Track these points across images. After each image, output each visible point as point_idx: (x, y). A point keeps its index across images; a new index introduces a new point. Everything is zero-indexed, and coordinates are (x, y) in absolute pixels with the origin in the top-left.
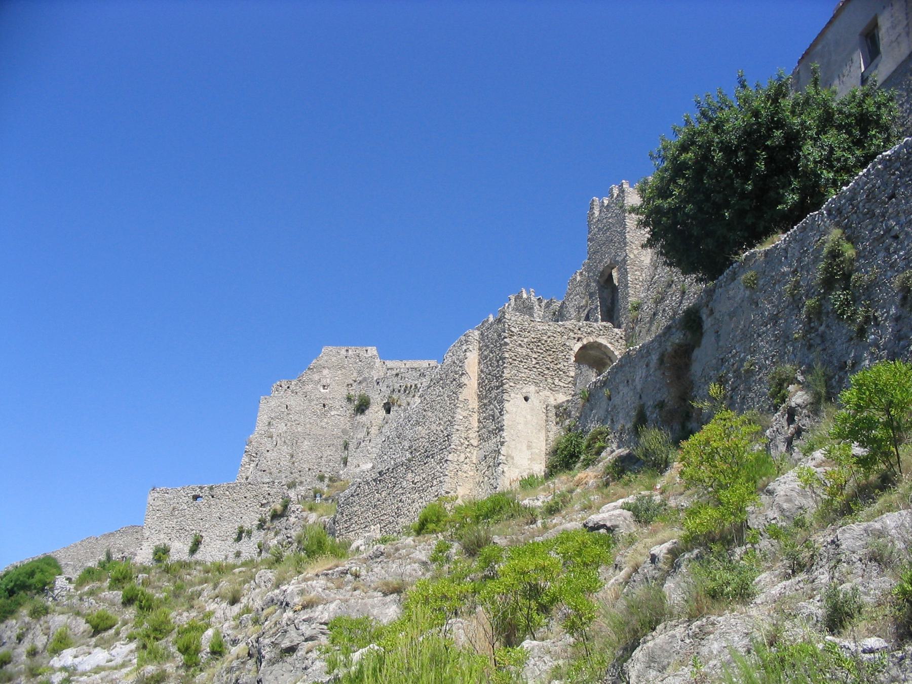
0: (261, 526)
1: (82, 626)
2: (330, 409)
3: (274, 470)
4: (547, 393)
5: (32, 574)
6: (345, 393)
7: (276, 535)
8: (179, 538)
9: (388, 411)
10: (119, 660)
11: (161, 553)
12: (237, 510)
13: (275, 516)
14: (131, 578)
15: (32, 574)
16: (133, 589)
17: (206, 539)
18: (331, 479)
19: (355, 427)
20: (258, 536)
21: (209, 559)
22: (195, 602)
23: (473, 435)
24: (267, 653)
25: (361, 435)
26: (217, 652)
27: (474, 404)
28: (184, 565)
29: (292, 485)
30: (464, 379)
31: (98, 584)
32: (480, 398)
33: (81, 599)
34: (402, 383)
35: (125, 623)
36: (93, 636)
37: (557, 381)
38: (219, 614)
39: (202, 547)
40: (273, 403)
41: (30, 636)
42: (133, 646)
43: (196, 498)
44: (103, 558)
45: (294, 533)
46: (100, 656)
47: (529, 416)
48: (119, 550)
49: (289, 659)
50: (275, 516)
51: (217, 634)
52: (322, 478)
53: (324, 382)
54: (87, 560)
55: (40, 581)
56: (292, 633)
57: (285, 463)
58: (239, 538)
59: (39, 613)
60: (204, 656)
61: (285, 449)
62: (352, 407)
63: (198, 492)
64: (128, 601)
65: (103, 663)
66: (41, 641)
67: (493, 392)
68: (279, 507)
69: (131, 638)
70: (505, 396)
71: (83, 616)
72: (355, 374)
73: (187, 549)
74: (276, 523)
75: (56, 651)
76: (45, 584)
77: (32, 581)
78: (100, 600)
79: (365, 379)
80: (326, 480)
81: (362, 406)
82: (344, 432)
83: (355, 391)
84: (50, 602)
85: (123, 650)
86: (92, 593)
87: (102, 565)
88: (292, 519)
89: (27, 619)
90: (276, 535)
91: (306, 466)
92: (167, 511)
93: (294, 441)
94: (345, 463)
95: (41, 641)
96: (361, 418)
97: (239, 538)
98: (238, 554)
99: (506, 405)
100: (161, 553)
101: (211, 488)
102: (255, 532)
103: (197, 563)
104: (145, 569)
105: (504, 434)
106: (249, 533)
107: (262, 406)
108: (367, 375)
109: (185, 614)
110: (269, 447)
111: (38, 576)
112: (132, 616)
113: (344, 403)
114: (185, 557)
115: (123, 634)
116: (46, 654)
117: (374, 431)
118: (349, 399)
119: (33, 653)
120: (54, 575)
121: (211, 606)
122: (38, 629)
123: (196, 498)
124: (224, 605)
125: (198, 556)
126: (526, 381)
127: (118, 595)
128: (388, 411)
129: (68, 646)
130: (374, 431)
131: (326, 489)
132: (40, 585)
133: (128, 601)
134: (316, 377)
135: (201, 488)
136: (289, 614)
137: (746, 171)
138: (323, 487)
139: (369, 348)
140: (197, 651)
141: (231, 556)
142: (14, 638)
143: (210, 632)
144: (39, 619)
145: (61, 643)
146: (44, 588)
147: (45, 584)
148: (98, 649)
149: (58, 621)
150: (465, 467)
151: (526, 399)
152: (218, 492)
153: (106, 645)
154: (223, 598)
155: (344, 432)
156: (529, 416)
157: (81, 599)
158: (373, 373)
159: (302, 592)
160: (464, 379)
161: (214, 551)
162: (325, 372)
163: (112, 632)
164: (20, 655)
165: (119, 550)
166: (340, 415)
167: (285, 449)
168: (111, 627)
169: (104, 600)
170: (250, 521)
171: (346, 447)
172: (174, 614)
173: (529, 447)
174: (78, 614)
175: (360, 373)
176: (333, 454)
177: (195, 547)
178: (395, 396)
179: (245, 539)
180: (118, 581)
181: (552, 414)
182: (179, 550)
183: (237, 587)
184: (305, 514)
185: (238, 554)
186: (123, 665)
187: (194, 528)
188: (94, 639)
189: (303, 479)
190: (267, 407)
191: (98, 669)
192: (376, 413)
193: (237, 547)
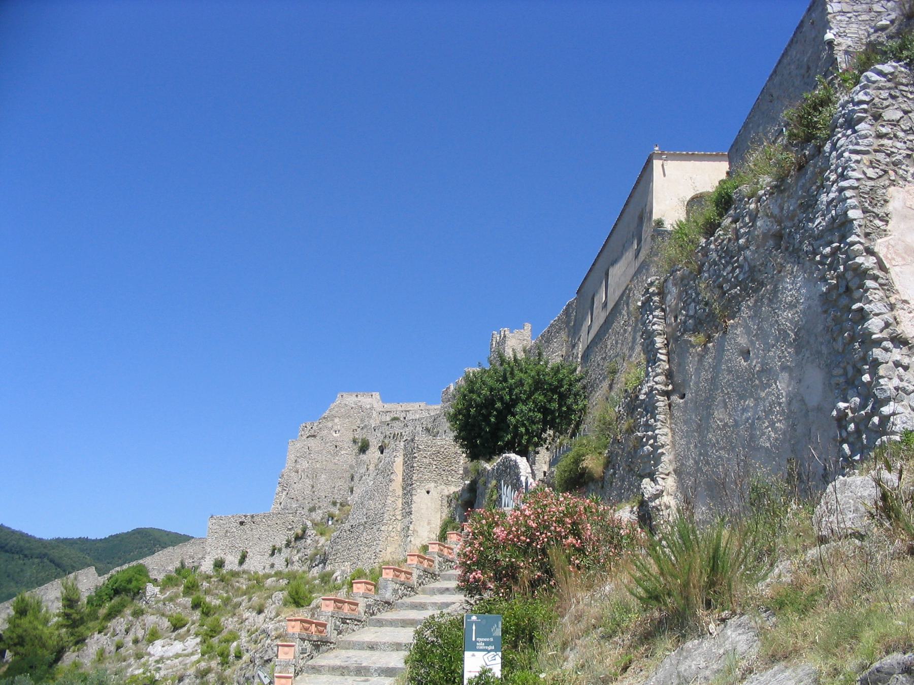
0: (288, 545)
1: (166, 623)
2: (341, 449)
3: (300, 498)
4: (443, 487)
5: (130, 581)
6: (351, 437)
7: (298, 552)
8: (231, 553)
9: (382, 453)
10: (189, 650)
11: (219, 564)
12: (271, 532)
13: (298, 538)
14: (198, 586)
15: (130, 581)
16: (198, 598)
17: (250, 554)
18: (341, 504)
19: (359, 464)
20: (286, 553)
21: (252, 569)
22: (237, 611)
23: (398, 512)
24: (258, 662)
25: (363, 471)
26: (238, 657)
27: (400, 492)
28: (235, 574)
29: (312, 510)
30: (392, 477)
31: (175, 590)
32: (404, 489)
33: (164, 604)
34: (392, 431)
35: (193, 623)
36: (173, 631)
37: (450, 478)
38: (251, 620)
39: (247, 560)
40: (298, 445)
41: (133, 630)
42: (198, 640)
43: (242, 523)
44: (178, 565)
45: (309, 552)
46: (178, 647)
47: (429, 504)
48: (190, 557)
49: (268, 666)
50: (298, 538)
51: (238, 645)
52: (334, 504)
53: (335, 428)
54: (168, 565)
55: (136, 587)
56: (270, 652)
57: (308, 492)
58: (273, 554)
59: (138, 613)
60: (231, 658)
61: (308, 482)
62: (356, 448)
63: (243, 519)
64: (196, 606)
65: (180, 652)
66: (140, 634)
67: (408, 488)
68: (300, 532)
69: (197, 635)
70: (414, 492)
71: (167, 616)
72: (359, 422)
73: (237, 561)
74: (298, 543)
75: (151, 641)
76: (140, 589)
77: (131, 586)
78: (176, 604)
79: (366, 426)
80: (338, 505)
81: (364, 448)
82: (351, 467)
83: (359, 435)
84: (143, 605)
85: (192, 642)
86: (171, 599)
87: (178, 571)
88: (309, 541)
89: (131, 618)
90: (298, 552)
91: (323, 495)
92: (222, 533)
93: (314, 475)
94: (352, 492)
95: (140, 634)
96: (363, 457)
97: (273, 554)
98: (272, 566)
99: (414, 497)
100: (219, 564)
101: (252, 517)
102: (284, 549)
103: (244, 572)
104: (208, 578)
105: (412, 517)
106: (280, 550)
107: (290, 447)
108: (367, 423)
109: (230, 619)
110: (296, 480)
111: (134, 583)
112: (198, 617)
113: (351, 444)
114: (236, 568)
115: (192, 632)
116: (145, 642)
117: (371, 467)
118: (355, 441)
119: (136, 641)
120: (145, 583)
121: (246, 615)
122: (138, 625)
123: (242, 523)
124: (254, 614)
125: (245, 566)
126: (428, 481)
127: (188, 601)
128: (382, 453)
129: (157, 638)
130: (371, 467)
131: (337, 512)
132: (136, 590)
133: (196, 606)
134: (330, 424)
135: (246, 516)
136: (269, 641)
137: (486, 418)
138: (336, 511)
139: (374, 393)
140: (228, 656)
141: (268, 566)
142: (123, 631)
143: (235, 644)
144: (138, 618)
145: (153, 636)
146: (138, 593)
147: (140, 589)
148: (177, 642)
149: (151, 619)
150: (392, 534)
151: (428, 492)
152: (256, 519)
153: (181, 638)
154: (254, 609)
155: (351, 467)
156: (429, 504)
157: (164, 604)
158: (371, 421)
159: (276, 629)
160: (392, 477)
161: (257, 564)
162: (337, 420)
163: (185, 629)
164: (128, 642)
165: (190, 557)
166: (348, 453)
167: (308, 482)
168: (184, 626)
169: (179, 605)
170: (280, 542)
171: (352, 479)
172: (223, 619)
173: (429, 524)
174: (163, 615)
175: (362, 421)
176: (343, 484)
177: (242, 561)
178: (386, 441)
179: (277, 555)
180: (190, 589)
181: (445, 503)
182: (231, 562)
183: (263, 601)
184: (317, 538)
185: (272, 566)
186: (192, 654)
187: (242, 546)
188: (174, 634)
189: (320, 504)
190: (294, 448)
191: (177, 656)
192: (373, 453)
193: (272, 560)
